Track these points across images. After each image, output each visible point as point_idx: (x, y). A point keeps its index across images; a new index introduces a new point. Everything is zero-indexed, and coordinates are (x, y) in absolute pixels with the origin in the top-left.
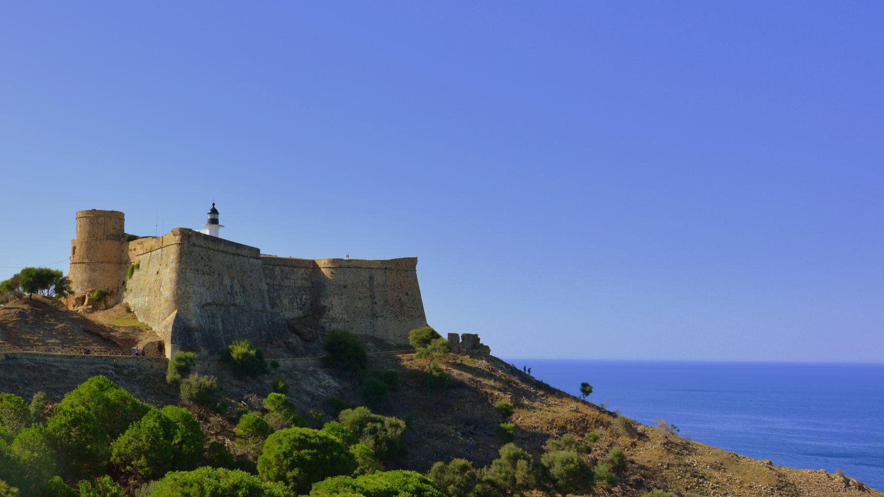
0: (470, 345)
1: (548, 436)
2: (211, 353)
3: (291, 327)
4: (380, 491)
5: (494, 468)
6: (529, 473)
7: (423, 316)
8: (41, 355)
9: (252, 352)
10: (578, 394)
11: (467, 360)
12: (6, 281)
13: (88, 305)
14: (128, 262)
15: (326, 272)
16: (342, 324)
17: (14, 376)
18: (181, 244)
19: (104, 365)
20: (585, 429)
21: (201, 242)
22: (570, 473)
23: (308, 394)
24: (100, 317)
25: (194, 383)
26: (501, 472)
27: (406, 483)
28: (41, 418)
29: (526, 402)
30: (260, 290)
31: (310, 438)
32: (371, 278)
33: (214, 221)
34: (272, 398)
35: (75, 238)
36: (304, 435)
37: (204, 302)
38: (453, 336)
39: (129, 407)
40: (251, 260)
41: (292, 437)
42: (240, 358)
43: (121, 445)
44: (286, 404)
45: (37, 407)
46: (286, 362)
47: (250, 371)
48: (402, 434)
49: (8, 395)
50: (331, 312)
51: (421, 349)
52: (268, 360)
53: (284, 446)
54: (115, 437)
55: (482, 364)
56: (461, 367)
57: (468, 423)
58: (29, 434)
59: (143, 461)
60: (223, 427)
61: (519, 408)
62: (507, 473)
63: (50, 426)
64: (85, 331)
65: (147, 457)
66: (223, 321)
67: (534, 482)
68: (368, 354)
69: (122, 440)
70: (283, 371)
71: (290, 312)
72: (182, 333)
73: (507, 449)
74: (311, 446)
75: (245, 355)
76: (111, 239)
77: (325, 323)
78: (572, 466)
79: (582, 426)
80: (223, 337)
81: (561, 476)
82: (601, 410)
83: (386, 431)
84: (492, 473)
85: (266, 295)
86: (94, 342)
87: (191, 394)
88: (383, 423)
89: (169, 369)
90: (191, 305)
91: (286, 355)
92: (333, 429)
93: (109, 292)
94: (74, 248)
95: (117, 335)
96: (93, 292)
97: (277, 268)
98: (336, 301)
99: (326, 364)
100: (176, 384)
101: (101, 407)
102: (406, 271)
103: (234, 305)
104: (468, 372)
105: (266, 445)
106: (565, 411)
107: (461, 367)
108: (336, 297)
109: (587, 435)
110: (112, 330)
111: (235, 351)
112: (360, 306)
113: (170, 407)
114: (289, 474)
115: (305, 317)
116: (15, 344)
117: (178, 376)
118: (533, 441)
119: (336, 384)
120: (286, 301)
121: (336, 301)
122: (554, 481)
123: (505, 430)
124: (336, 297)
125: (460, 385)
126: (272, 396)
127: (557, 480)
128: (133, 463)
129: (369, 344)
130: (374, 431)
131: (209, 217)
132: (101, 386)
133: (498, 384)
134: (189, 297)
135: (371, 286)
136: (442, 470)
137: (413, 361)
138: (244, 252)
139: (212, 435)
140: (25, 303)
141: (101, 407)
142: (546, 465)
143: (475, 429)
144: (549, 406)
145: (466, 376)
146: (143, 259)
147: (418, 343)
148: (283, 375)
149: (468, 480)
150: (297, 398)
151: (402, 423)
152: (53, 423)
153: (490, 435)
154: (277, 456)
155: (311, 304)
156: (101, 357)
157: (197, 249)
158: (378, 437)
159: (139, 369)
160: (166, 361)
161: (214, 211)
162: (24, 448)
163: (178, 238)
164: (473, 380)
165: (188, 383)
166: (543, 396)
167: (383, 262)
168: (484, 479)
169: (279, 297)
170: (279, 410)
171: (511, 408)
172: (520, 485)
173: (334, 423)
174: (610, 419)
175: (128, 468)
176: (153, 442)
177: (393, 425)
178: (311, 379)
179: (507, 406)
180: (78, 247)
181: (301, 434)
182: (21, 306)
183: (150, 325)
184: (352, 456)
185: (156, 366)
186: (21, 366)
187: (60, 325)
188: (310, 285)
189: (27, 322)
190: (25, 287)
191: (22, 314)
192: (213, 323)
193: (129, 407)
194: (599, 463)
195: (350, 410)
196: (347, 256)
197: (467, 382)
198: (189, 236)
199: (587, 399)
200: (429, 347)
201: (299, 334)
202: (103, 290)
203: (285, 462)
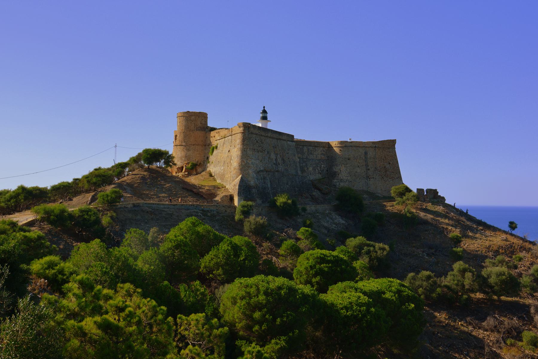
1: (486, 257)
2: (263, 202)
3: (314, 185)
4: (373, 291)
5: (449, 278)
6: (474, 281)
7: (400, 178)
8: (156, 204)
10: (507, 229)
11: (430, 206)
13: (185, 172)
14: (210, 144)
15: (337, 150)
16: (347, 183)
17: (139, 217)
18: (243, 133)
19: (195, 210)
20: (513, 253)
22: (503, 282)
23: (326, 228)
24: (193, 180)
25: (253, 221)
26: (454, 280)
27: (390, 286)
28: (155, 244)
29: (470, 234)
31: (327, 256)
32: (366, 153)
33: (264, 118)
34: (303, 231)
36: (323, 254)
37: (258, 170)
38: (420, 191)
39: (211, 237)
40: (289, 142)
41: (315, 256)
42: (282, 205)
43: (206, 261)
44: (311, 234)
46: (311, 208)
47: (289, 214)
48: (387, 254)
49: (134, 229)
51: (399, 199)
52: (300, 207)
53: (310, 262)
54: (203, 256)
55: (440, 209)
56: (426, 210)
58: (148, 254)
59: (220, 271)
60: (271, 249)
61: (466, 238)
62: (458, 281)
63: (162, 249)
64: (183, 188)
65: (223, 269)
66: (271, 181)
67: (477, 287)
68: (364, 202)
69: (207, 258)
70: (309, 214)
71: (313, 175)
72: (245, 189)
73: (458, 265)
74: (328, 262)
75: (285, 203)
76: (199, 130)
78: (504, 277)
79: (510, 251)
81: (496, 284)
82: (524, 240)
83: (376, 252)
84: (448, 280)
86: (190, 195)
87: (251, 229)
88: (374, 247)
89: (236, 212)
90: (250, 171)
94: (176, 136)
95: (204, 191)
96: (188, 163)
98: (343, 168)
99: (337, 209)
100: (241, 222)
102: (389, 148)
104: (430, 214)
106: (498, 240)
107: (426, 210)
108: (343, 166)
109: (514, 257)
110: (200, 188)
111: (278, 201)
112: (359, 171)
113: (237, 236)
114: (314, 280)
115: (323, 178)
117: (242, 217)
118: (476, 260)
119: (344, 222)
120: (311, 169)
121: (343, 168)
122: (491, 287)
124: (343, 166)
125: (425, 222)
126: (303, 229)
127: (494, 287)
128: (214, 272)
129: (365, 196)
130: (368, 253)
131: (261, 115)
132: (193, 224)
133: (451, 222)
134: (249, 167)
136: (414, 278)
137: (394, 207)
138: (284, 138)
139: (264, 254)
140: (145, 171)
141: (194, 236)
142: (485, 276)
144: (486, 236)
145: (430, 217)
146: (220, 143)
148: (310, 216)
149: (431, 285)
151: (387, 247)
154: (306, 268)
155: (327, 171)
156: (194, 205)
157: (254, 136)
158: (371, 256)
160: (235, 207)
161: (264, 112)
162: (145, 263)
163: (242, 129)
164: (434, 219)
165: (249, 221)
166: (482, 230)
167: (373, 143)
168: (443, 284)
170: (307, 238)
171: (460, 238)
172: (468, 289)
173: (343, 247)
174: (531, 246)
175: (211, 275)
176: (227, 259)
177: (381, 248)
179: (457, 236)
180: (178, 136)
181: (321, 254)
182: (142, 173)
183: (224, 184)
184: (354, 268)
185: (228, 210)
188: (326, 158)
189: (146, 183)
191: (143, 178)
192: (265, 183)
193: (211, 237)
194: (524, 276)
195: (353, 238)
196: (350, 139)
197: (430, 220)
198: (249, 127)
199: (514, 232)
200: (404, 198)
201: (319, 190)
202: (195, 162)
203: (311, 272)
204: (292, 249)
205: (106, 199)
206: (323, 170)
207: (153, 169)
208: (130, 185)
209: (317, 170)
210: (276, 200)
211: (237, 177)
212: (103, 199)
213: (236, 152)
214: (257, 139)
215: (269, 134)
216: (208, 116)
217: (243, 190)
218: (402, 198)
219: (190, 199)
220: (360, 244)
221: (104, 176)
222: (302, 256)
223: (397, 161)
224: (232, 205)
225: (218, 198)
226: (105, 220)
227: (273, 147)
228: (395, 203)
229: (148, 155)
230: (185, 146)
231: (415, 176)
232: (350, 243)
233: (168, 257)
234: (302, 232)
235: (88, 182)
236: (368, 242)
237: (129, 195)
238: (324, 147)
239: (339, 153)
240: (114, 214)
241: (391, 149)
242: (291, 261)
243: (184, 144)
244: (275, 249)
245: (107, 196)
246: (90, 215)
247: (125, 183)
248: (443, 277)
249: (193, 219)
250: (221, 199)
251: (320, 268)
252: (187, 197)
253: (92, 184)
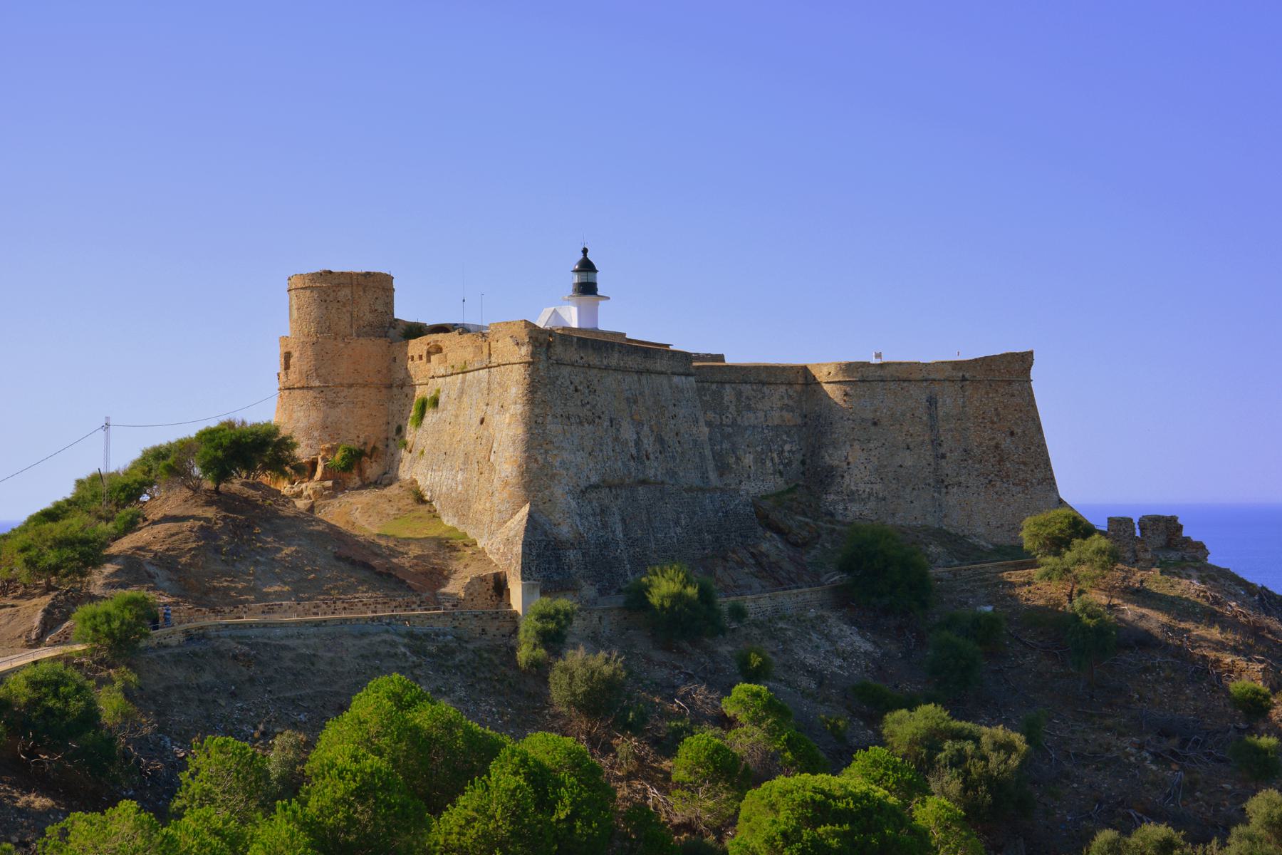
0: (1160, 540)
2: (602, 592)
3: (764, 516)
8: (257, 625)
9: (691, 591)
11: (1156, 581)
12: (160, 447)
13: (323, 479)
14: (406, 384)
16: (872, 504)
17: (207, 677)
18: (531, 365)
19: (386, 637)
21: (573, 355)
23: (811, 672)
24: (359, 514)
25: (580, 672)
28: (293, 785)
30: (695, 441)
31: (835, 798)
32: (932, 402)
33: (587, 289)
34: (743, 696)
35: (287, 332)
36: (823, 792)
37: (583, 484)
38: (1119, 525)
40: (676, 379)
41: (797, 797)
42: (667, 604)
44: (771, 706)
45: (284, 763)
46: (758, 603)
47: (686, 626)
48: (1022, 763)
49: (220, 740)
50: (847, 477)
51: (1050, 559)
52: (724, 603)
53: (782, 817)
54: (437, 810)
55: (1189, 588)
56: (1142, 596)
57: (1165, 733)
60: (641, 760)
63: (313, 807)
64: (338, 558)
66: (623, 520)
68: (933, 572)
69: (453, 817)
70: (755, 624)
71: (757, 480)
72: (543, 555)
74: (839, 817)
75: (677, 598)
76: (367, 334)
77: (834, 503)
80: (625, 556)
83: (985, 758)
85: (708, 452)
86: (362, 583)
87: (574, 694)
88: (977, 740)
89: (521, 636)
90: (558, 491)
91: (756, 583)
92: (876, 764)
93: (368, 450)
94: (288, 356)
95: (405, 562)
96: (333, 450)
97: (727, 386)
98: (856, 455)
99: (843, 600)
100: (540, 670)
101: (403, 746)
102: (1010, 382)
103: (644, 482)
104: (1158, 609)
105: (743, 814)
107: (1142, 596)
108: (857, 446)
110: (394, 553)
111: (655, 591)
112: (909, 462)
113: (540, 735)
115: (790, 491)
116: (199, 603)
117: (541, 653)
120: (748, 460)
121: (856, 455)
123: (1258, 751)
124: (857, 446)
125: (1143, 640)
129: (932, 549)
130: (958, 761)
131: (576, 279)
132: (396, 698)
133: (1230, 637)
134: (553, 477)
135: (933, 418)
137: (1040, 587)
139: (620, 779)
140: (209, 503)
141: (403, 746)
143: (1183, 744)
145: (1155, 620)
146: (448, 388)
147: (1043, 545)
148: (755, 631)
150: (789, 684)
151: (1018, 739)
152: (321, 798)
153: (1220, 760)
154: (770, 841)
155: (803, 463)
156: (380, 619)
157: (565, 371)
158: (968, 772)
159: (458, 639)
161: (587, 266)
163: (525, 350)
164: (1171, 628)
165: (565, 670)
167: (957, 365)
169: (734, 449)
170: (756, 721)
171: (1266, 697)
173: (876, 752)
177: (998, 742)
178: (814, 636)
179: (1257, 692)
180: (296, 355)
181: (815, 790)
182: (199, 512)
183: (471, 534)
185: (492, 628)
186: (220, 654)
187: (287, 551)
188: (799, 421)
189: (218, 550)
190: (206, 468)
193: (460, 742)
195: (904, 711)
196: (878, 356)
197: (1156, 631)
198: (549, 345)
200: (1069, 556)
201: (779, 531)
202: (355, 445)
204: (714, 763)
205: (105, 628)
206: (790, 463)
207: (233, 497)
208: (166, 561)
209: (769, 464)
210: (646, 588)
211: (514, 513)
212: (95, 630)
213: (507, 428)
214: (574, 370)
215: (614, 360)
216: (396, 284)
217: (538, 555)
218: (1058, 554)
219: (364, 594)
220: (930, 729)
221: (84, 542)
222: (753, 795)
223: (1043, 445)
224: (504, 609)
225: (455, 587)
226: (110, 704)
227: (628, 399)
228: (1036, 573)
229: (216, 450)
230: (321, 390)
231: (1100, 461)
232: (898, 729)
233: (337, 828)
234: (740, 702)
235: (30, 563)
236: (956, 724)
237: (167, 600)
238: (790, 384)
239: (842, 403)
240: (133, 678)
241: (1016, 386)
242: (710, 803)
243: (317, 384)
244: (651, 758)
245: (108, 617)
246: (66, 699)
247: (149, 555)
248: (1215, 841)
249: (393, 681)
250: (467, 588)
251: (813, 840)
252: (352, 588)
253: (44, 570)
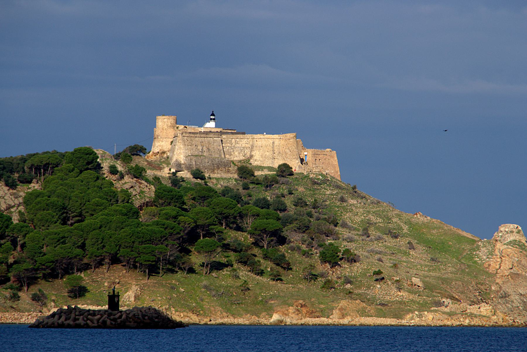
32: (273, 143)
120: (236, 153)
169: (233, 151)
